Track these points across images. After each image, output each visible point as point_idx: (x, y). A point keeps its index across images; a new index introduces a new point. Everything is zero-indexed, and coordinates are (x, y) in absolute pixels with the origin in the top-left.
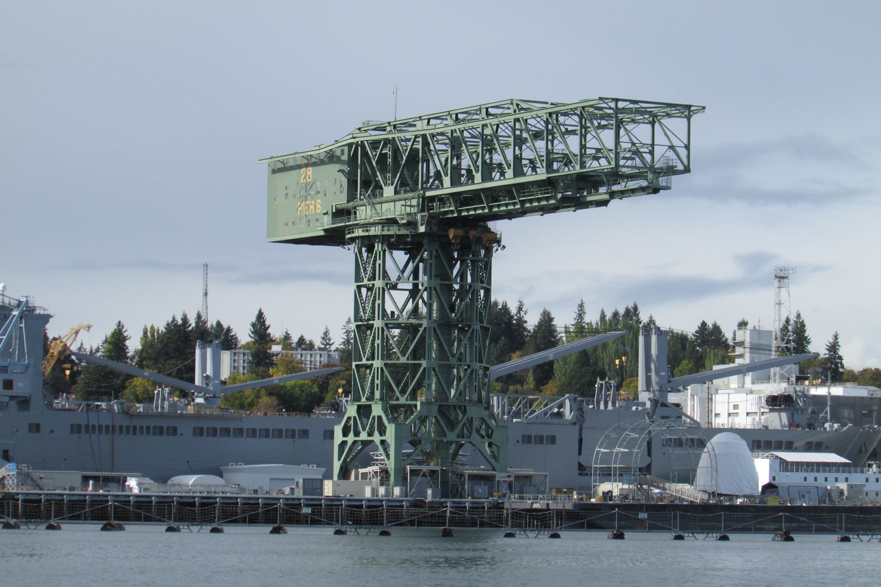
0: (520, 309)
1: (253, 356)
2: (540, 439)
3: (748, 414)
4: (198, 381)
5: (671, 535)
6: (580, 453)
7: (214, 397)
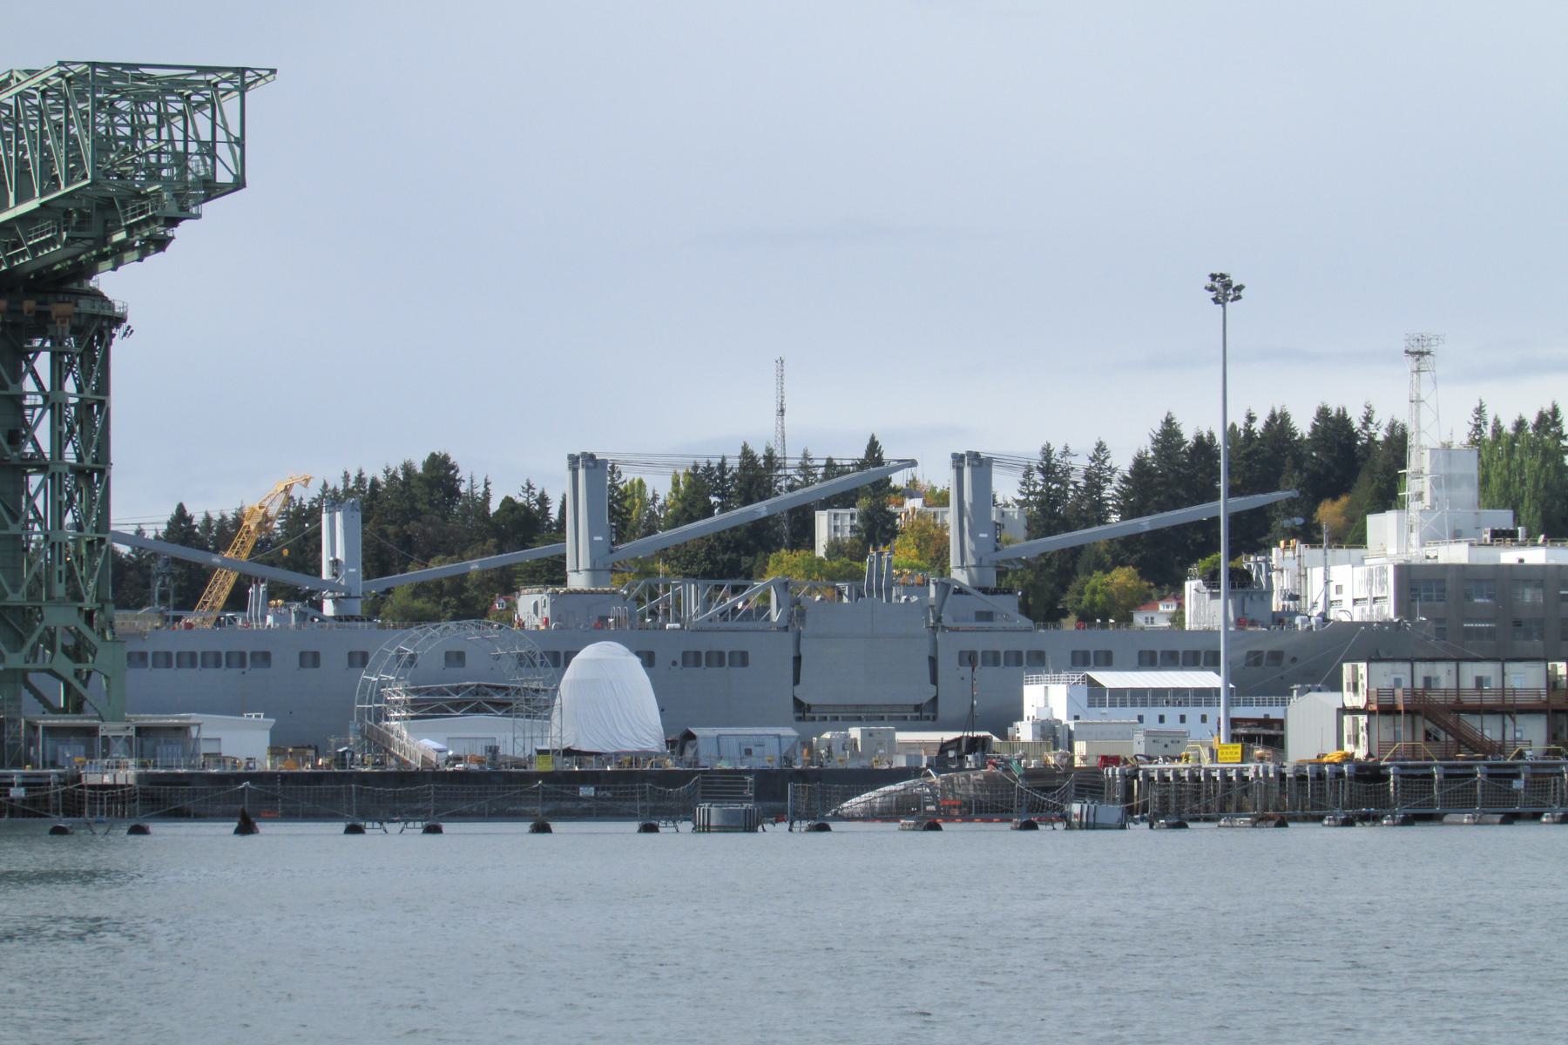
0: (1368, 419)
1: (861, 519)
2: (717, 659)
3: (1355, 601)
4: (326, 574)
5: (634, 826)
6: (796, 681)
7: (348, 597)
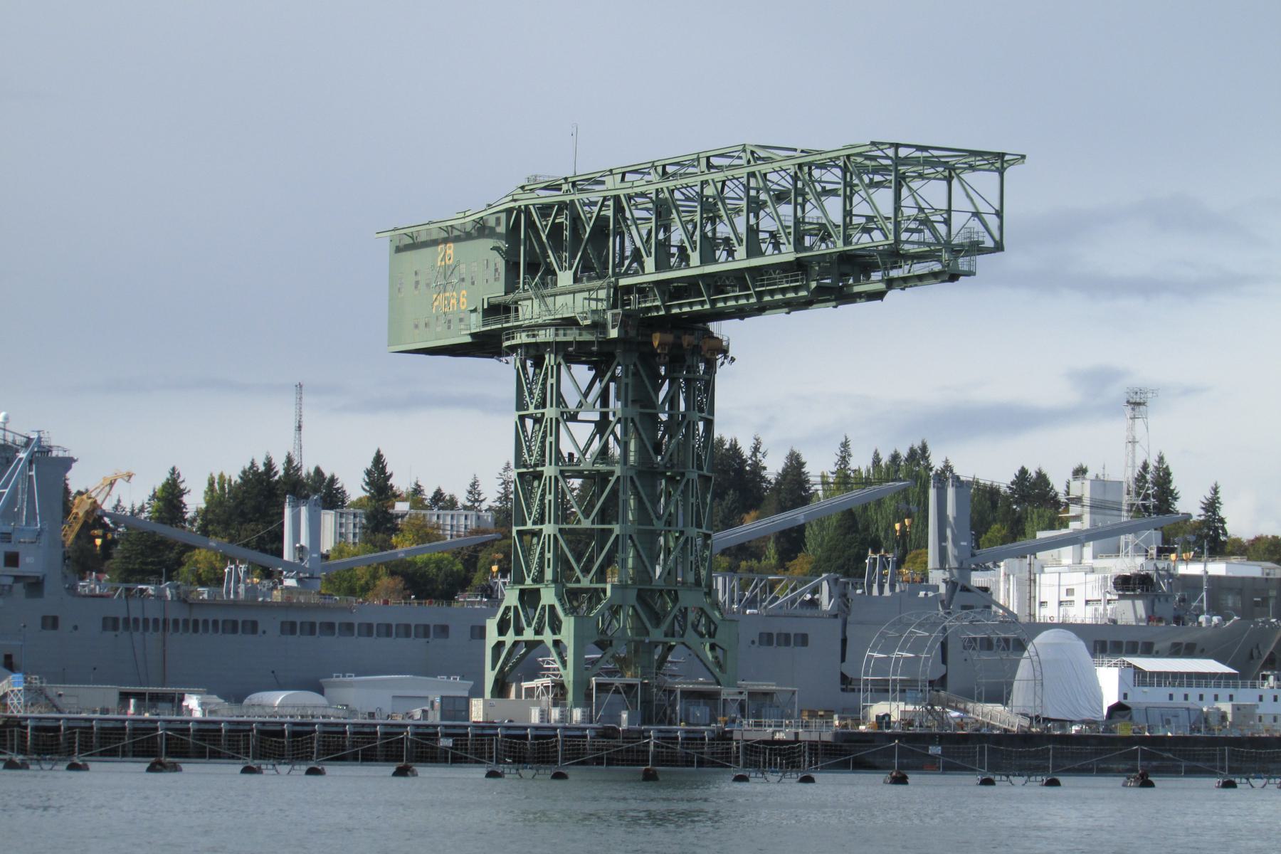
0: (756, 450)
1: (368, 518)
2: (785, 639)
3: (1087, 602)
4: (288, 555)
5: (975, 779)
6: (843, 660)
7: (311, 577)
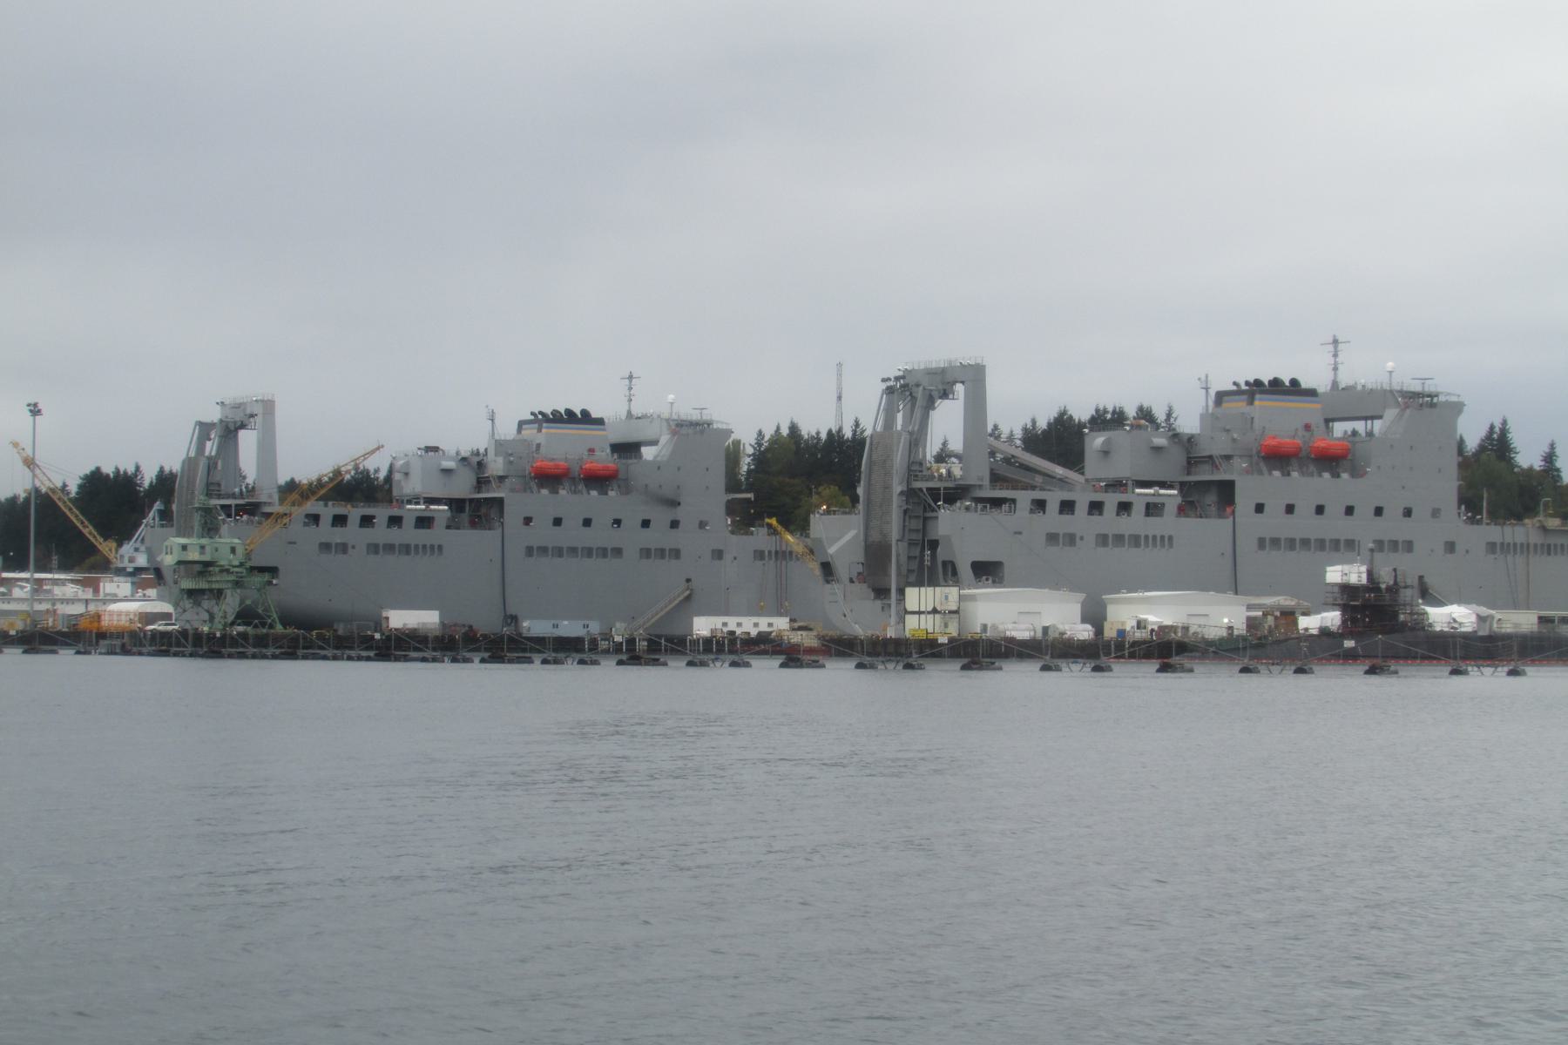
0: (1169, 415)
2: (661, 553)
